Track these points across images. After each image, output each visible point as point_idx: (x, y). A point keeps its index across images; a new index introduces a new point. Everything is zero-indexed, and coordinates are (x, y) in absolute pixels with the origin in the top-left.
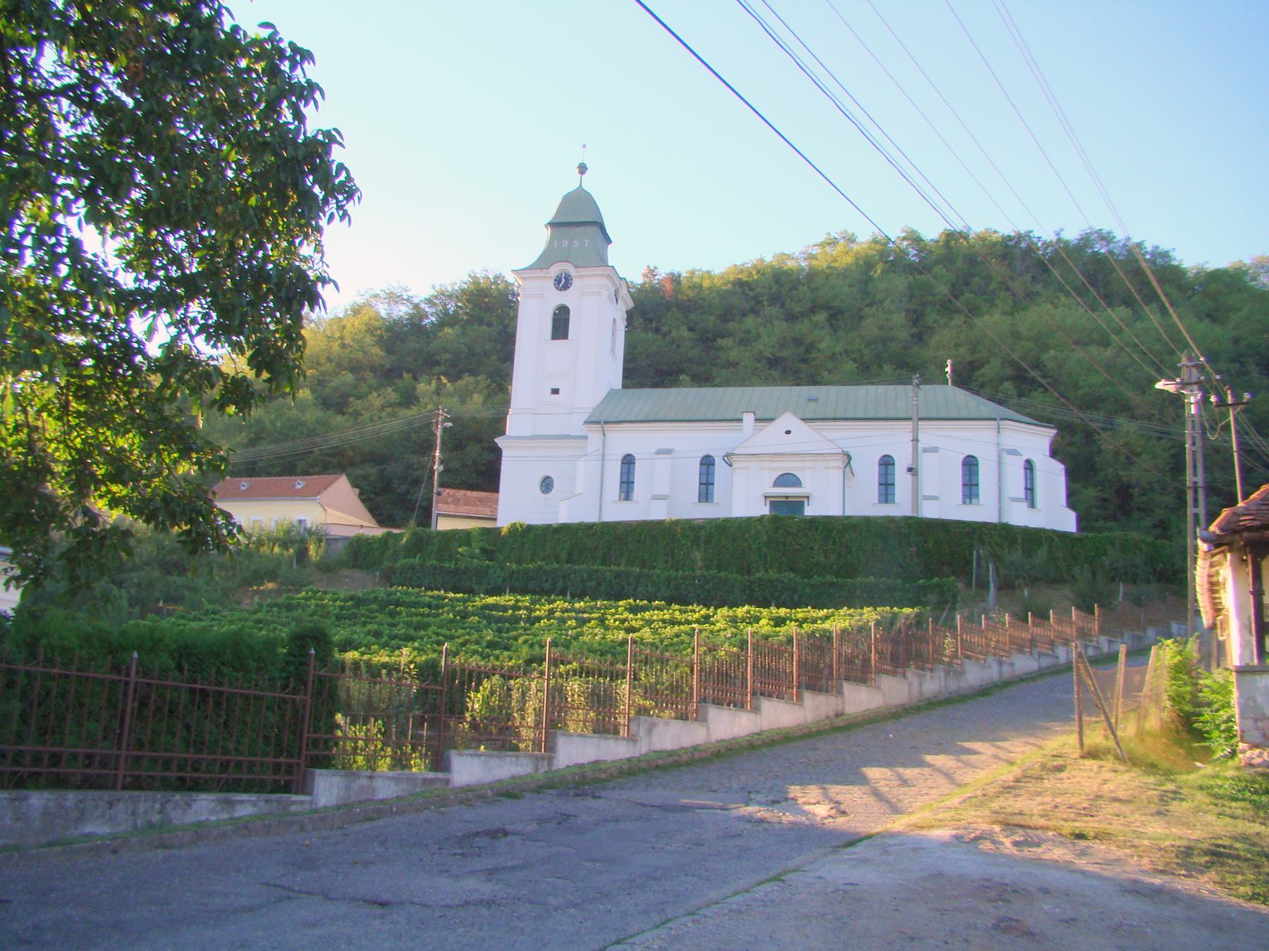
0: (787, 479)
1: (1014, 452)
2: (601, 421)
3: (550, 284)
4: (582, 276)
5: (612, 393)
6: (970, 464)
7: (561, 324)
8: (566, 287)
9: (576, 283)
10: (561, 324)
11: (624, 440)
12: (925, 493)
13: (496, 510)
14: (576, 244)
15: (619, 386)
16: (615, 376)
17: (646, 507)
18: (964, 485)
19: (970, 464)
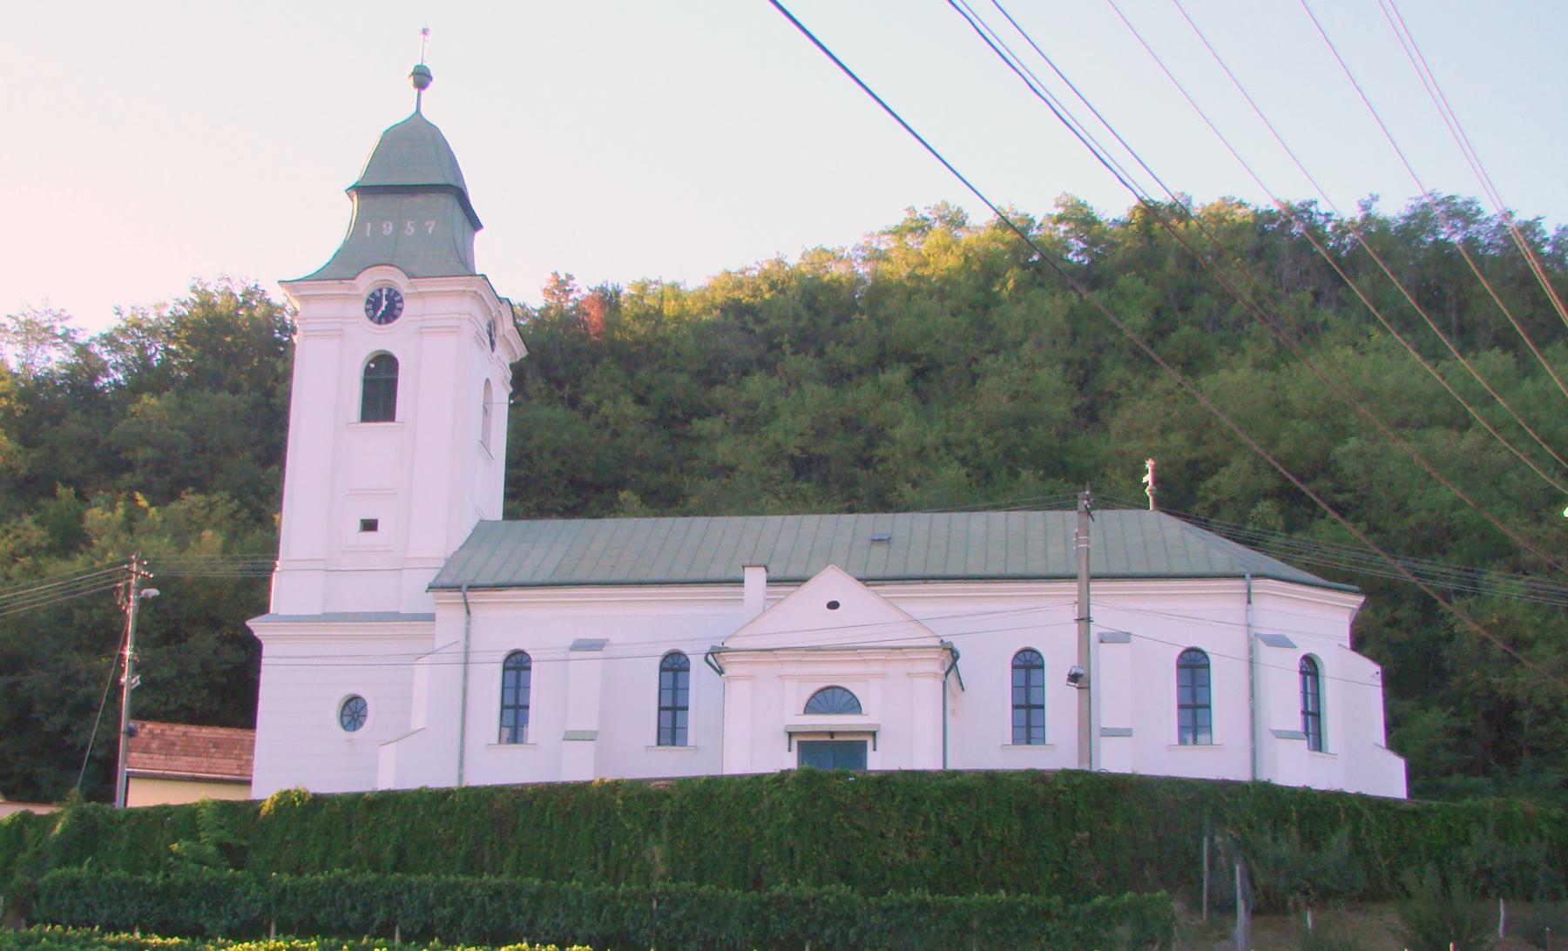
2: (461, 584)
3: (359, 309)
4: (421, 295)
5: (482, 530)
6: (1193, 665)
7: (380, 391)
8: (390, 315)
9: (410, 308)
10: (380, 391)
11: (508, 623)
14: (410, 229)
19: (1193, 665)
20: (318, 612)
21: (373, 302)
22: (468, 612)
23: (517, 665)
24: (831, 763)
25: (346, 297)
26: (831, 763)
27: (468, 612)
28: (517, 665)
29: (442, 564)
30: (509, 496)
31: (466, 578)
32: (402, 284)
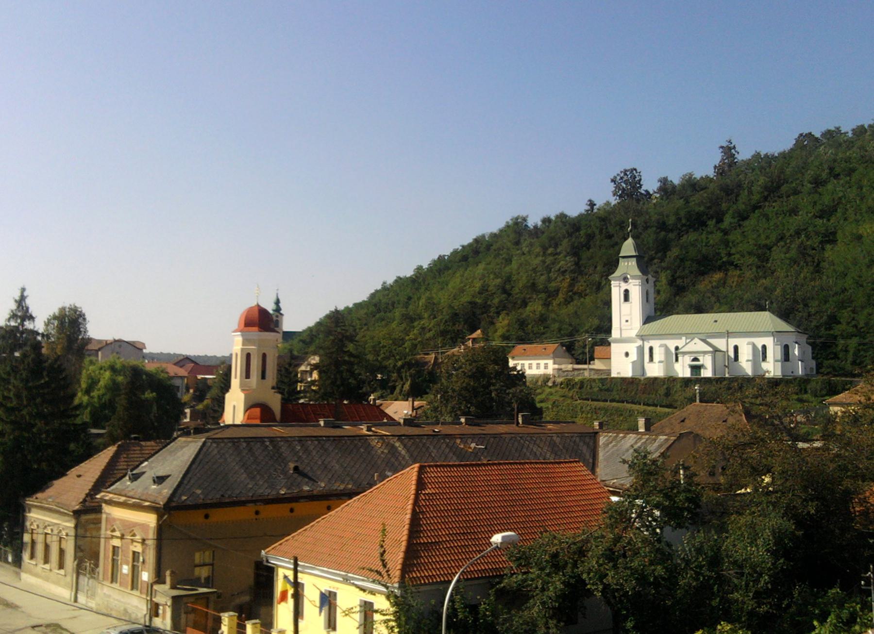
6: (764, 347)
13: (773, 313)
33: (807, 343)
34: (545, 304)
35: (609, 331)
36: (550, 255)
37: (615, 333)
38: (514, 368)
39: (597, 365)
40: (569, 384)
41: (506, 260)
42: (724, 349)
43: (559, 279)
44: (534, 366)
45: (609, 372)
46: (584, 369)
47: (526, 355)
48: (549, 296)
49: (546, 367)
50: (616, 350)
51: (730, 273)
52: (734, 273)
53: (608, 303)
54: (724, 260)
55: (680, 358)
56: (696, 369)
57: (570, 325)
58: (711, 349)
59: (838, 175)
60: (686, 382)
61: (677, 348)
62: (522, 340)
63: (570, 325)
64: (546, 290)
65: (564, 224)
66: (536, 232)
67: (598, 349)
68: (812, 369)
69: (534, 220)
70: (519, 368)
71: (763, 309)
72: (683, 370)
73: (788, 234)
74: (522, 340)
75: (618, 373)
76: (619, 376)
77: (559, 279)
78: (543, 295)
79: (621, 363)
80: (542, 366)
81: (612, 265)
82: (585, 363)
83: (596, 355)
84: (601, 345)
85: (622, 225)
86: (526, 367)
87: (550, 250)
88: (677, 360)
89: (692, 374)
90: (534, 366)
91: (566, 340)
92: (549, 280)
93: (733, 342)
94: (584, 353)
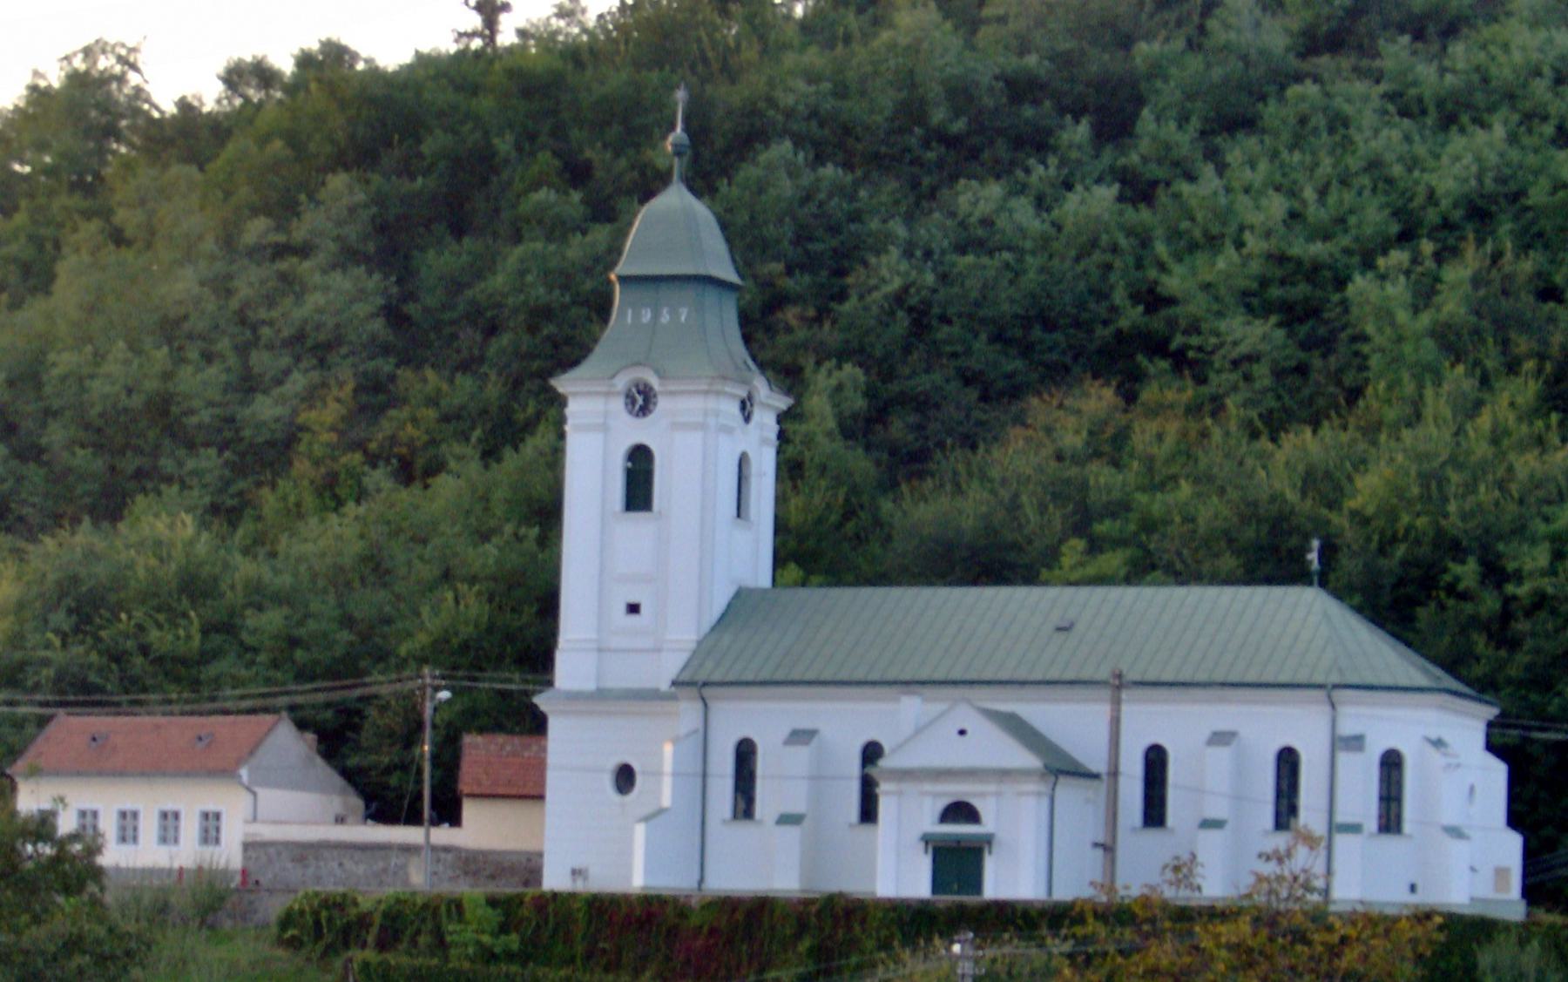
0: (960, 811)
1: (1356, 743)
2: (696, 684)
3: (618, 404)
4: (672, 393)
5: (742, 604)
6: (1288, 762)
7: (639, 483)
8: (644, 410)
9: (663, 404)
10: (639, 483)
11: (737, 718)
12: (695, 885)
13: (1339, 594)
14: (665, 318)
15: (765, 580)
16: (750, 554)
17: (761, 863)
18: (1381, 799)
19: (1288, 762)
20: (590, 686)
21: (630, 399)
22: (706, 705)
23: (745, 754)
24: (955, 899)
25: (608, 394)
26: (955, 899)
27: (706, 705)
28: (745, 754)
29: (693, 646)
30: (779, 561)
31: (702, 676)
32: (654, 382)
33: (1491, 747)
34: (214, 509)
35: (538, 657)
36: (253, 252)
37: (572, 667)
38: (42, 827)
39: (482, 828)
40: (325, 926)
41: (26, 269)
42: (1099, 765)
43: (298, 382)
44: (149, 827)
45: (531, 868)
46: (408, 849)
47: (100, 764)
48: (239, 470)
49: (211, 826)
50: (573, 747)
51: (1149, 394)
52: (1164, 388)
53: (545, 514)
54: (1124, 323)
55: (885, 806)
56: (957, 860)
57: (347, 621)
58: (1028, 760)
59: (1053, 224)
60: (914, 923)
61: (871, 753)
62: (1177, 574)
63: (347, 621)
64: (225, 434)
65: (331, 88)
66: (190, 134)
67: (477, 749)
68: (1501, 873)
69: (180, 75)
70: (66, 824)
71: (1294, 574)
72: (897, 871)
73: (1432, 216)
74: (80, 693)
75: (575, 873)
76: (580, 886)
77: (298, 382)
78: (209, 461)
79: (600, 814)
80: (190, 828)
81: (567, 327)
82: (414, 819)
83: (469, 775)
84: (498, 727)
85: (632, 122)
86: (108, 825)
87: (257, 229)
88: (868, 812)
89: (938, 885)
90: (149, 827)
91: (313, 696)
92: (248, 385)
93: (1148, 720)
94: (407, 767)
